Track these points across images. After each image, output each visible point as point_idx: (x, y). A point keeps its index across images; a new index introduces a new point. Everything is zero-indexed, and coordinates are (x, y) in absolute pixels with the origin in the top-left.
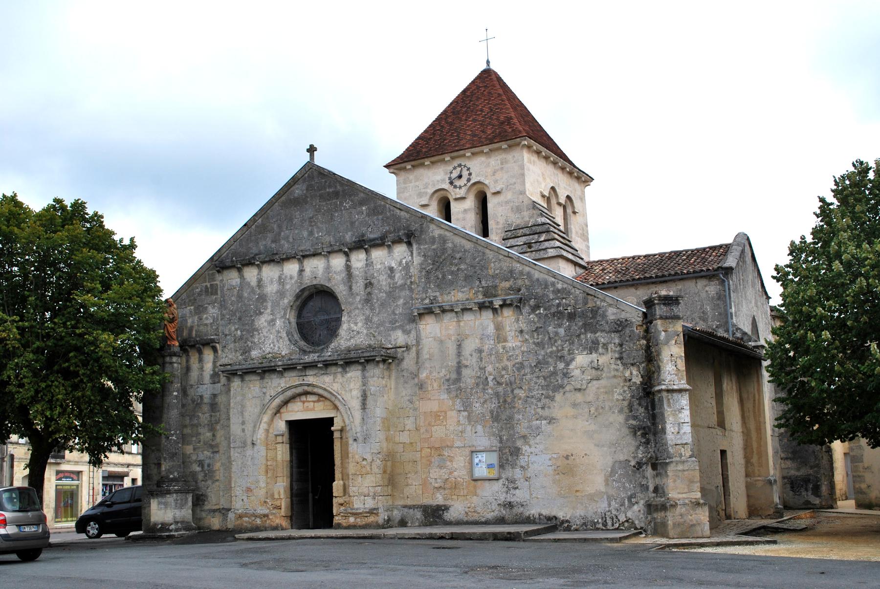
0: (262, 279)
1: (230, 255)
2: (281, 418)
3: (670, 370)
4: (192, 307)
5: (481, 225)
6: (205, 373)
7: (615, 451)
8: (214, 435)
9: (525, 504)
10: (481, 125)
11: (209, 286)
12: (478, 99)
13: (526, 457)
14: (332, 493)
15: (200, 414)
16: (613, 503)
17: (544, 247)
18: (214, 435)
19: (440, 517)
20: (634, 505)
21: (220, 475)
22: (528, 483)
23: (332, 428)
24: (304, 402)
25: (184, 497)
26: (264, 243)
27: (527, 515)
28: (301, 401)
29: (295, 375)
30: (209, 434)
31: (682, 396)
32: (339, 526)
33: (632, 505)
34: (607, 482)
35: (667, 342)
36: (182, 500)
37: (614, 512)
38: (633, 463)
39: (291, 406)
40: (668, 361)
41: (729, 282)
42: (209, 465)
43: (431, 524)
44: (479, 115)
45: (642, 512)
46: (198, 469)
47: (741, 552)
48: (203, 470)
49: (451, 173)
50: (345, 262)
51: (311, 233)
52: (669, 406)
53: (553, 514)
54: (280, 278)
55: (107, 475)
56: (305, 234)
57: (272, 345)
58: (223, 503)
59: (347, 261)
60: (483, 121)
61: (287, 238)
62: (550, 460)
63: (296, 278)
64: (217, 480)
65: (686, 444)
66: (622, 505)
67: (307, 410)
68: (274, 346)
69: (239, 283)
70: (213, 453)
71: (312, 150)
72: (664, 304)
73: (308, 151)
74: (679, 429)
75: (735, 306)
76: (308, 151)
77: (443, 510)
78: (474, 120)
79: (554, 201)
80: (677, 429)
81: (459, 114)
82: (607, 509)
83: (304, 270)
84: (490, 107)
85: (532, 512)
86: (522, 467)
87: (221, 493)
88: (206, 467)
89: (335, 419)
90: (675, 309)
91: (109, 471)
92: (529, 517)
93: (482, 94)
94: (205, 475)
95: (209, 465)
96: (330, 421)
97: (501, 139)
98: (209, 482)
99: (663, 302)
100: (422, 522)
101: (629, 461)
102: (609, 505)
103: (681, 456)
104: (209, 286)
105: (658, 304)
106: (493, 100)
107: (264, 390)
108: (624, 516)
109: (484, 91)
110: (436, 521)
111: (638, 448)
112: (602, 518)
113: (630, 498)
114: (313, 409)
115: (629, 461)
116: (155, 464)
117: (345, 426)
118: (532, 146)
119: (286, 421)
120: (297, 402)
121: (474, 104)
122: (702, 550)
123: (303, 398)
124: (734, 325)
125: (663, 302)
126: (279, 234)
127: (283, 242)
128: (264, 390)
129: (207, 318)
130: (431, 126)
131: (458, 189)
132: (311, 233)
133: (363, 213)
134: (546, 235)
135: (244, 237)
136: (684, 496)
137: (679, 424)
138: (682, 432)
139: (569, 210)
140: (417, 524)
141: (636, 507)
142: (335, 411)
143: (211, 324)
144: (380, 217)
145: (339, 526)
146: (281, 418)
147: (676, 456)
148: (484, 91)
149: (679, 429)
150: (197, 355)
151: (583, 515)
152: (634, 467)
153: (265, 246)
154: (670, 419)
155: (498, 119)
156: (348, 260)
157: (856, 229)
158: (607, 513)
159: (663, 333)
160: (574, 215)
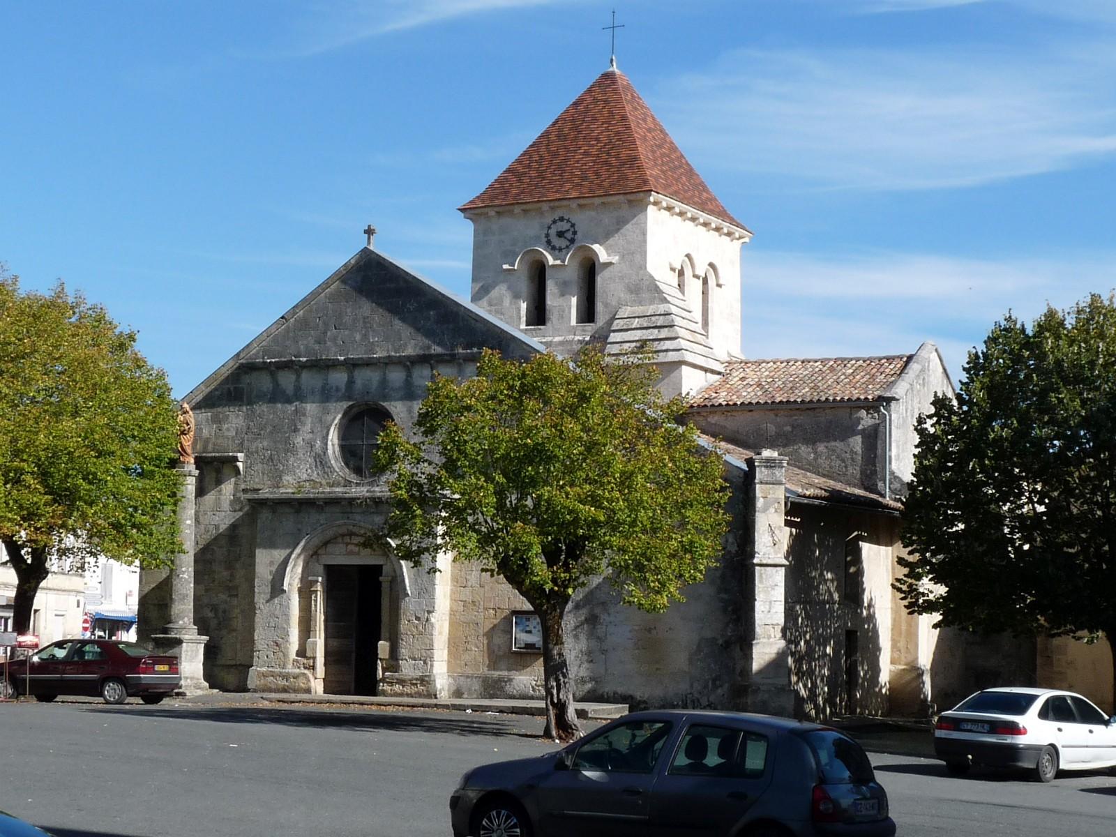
0: (300, 388)
1: (261, 353)
2: (318, 561)
3: (766, 541)
4: (209, 414)
5: (586, 303)
6: (223, 497)
7: (702, 628)
8: (232, 575)
9: (599, 680)
10: (594, 161)
11: (232, 389)
12: (595, 119)
13: (604, 627)
14: (377, 654)
15: (215, 548)
16: (696, 685)
17: (664, 348)
18: (232, 575)
19: (501, 689)
20: (717, 688)
21: (238, 623)
22: (604, 657)
23: (381, 578)
24: (347, 544)
25: (194, 648)
26: (305, 342)
27: (601, 692)
28: (344, 543)
29: (338, 510)
30: (226, 573)
31: (777, 571)
32: (384, 693)
33: (715, 687)
34: (691, 661)
35: (765, 510)
36: (192, 651)
37: (696, 695)
38: (720, 642)
39: (330, 548)
40: (763, 531)
41: (890, 416)
42: (224, 612)
43: (492, 697)
44: (593, 145)
45: (726, 696)
46: (210, 615)
47: (918, 759)
48: (216, 616)
49: (549, 228)
50: (404, 377)
51: (365, 336)
52: (761, 582)
53: (630, 692)
54: (323, 388)
55: (5, 604)
56: (358, 337)
57: (309, 471)
58: (240, 659)
59: (407, 376)
60: (597, 156)
61: (334, 339)
62: (630, 631)
63: (343, 390)
64: (234, 630)
65: (778, 624)
66: (706, 687)
67: (351, 553)
68: (313, 472)
69: (271, 388)
70: (230, 596)
71: (369, 232)
72: (766, 467)
73: (365, 232)
74: (770, 608)
75: (898, 447)
76: (365, 232)
77: (506, 682)
78: (586, 154)
79: (688, 273)
80: (768, 607)
81: (566, 140)
82: (689, 692)
83: (354, 382)
84: (609, 136)
85: (606, 690)
86: (598, 638)
87: (238, 647)
88: (220, 614)
89: (384, 567)
90: (777, 473)
91: (7, 597)
92: (602, 695)
93: (600, 112)
94: (219, 624)
95: (224, 612)
96: (378, 569)
97: (619, 190)
98: (224, 632)
99: (765, 464)
100: (481, 694)
101: (717, 640)
102: (692, 686)
103: (769, 637)
104: (232, 389)
105: (758, 466)
106: (614, 125)
107: (300, 526)
108: (706, 700)
109: (604, 108)
110: (497, 694)
111: (727, 625)
112: (683, 701)
113: (714, 680)
114: (358, 553)
115: (717, 640)
116: (155, 605)
117: (396, 577)
118: (661, 202)
119: (325, 566)
120: (339, 543)
121: (587, 127)
122: (923, 761)
123: (347, 539)
124: (892, 473)
125: (765, 464)
126: (325, 333)
127: (329, 343)
128: (300, 526)
129: (228, 429)
130: (525, 153)
131: (557, 252)
132: (365, 336)
133: (429, 320)
134: (669, 331)
135: (280, 332)
136: (769, 681)
137: (770, 602)
138: (773, 611)
139: (712, 282)
140: (475, 696)
141: (720, 691)
142: (385, 558)
143: (233, 437)
144: (451, 326)
145: (384, 693)
146: (318, 561)
147: (764, 637)
148: (604, 108)
149: (770, 608)
150: (214, 475)
151: (662, 695)
152: (722, 645)
153: (307, 346)
154: (761, 595)
155: (617, 157)
156: (409, 375)
157: (700, 555)
158: (688, 696)
159: (762, 500)
160: (718, 288)
